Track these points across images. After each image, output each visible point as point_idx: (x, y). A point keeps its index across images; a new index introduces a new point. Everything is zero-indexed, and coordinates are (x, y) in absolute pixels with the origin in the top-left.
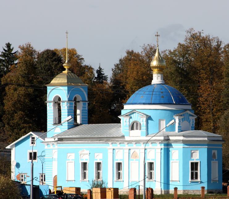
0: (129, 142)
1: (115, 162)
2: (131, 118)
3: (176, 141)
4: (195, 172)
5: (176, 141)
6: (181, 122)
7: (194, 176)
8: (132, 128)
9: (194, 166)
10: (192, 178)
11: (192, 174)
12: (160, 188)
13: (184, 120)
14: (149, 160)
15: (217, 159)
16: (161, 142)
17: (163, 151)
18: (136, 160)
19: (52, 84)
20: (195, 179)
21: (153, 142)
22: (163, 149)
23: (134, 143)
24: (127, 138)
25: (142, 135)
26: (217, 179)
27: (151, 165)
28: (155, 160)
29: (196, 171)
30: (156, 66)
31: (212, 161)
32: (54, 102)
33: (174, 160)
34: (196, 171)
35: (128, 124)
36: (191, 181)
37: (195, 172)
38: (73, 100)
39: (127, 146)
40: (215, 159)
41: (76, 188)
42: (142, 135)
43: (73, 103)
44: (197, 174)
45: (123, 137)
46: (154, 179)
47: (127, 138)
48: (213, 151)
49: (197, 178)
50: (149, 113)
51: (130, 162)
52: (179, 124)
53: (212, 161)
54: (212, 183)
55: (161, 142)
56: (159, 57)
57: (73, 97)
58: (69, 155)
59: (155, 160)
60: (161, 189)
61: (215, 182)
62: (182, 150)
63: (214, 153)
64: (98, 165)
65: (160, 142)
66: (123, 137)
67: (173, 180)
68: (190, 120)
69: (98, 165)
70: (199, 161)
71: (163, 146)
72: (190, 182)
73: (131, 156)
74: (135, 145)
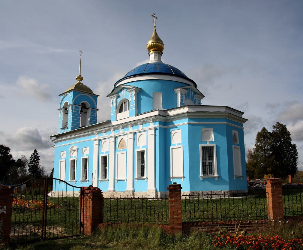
0: (116, 128)
1: (101, 155)
2: (119, 97)
3: (179, 117)
4: (208, 162)
5: (179, 117)
6: (184, 97)
7: (207, 168)
8: (121, 111)
9: (208, 152)
10: (204, 172)
11: (204, 165)
12: (154, 188)
13: (188, 98)
14: (140, 147)
15: (238, 143)
16: (154, 117)
17: (157, 132)
18: (123, 151)
19: (138, 147)
20: (209, 174)
21: (144, 122)
22: (158, 128)
23: (120, 127)
24: (114, 123)
25: (130, 115)
26: (241, 174)
27: (142, 154)
28: (146, 146)
29: (210, 161)
30: (152, 43)
31: (233, 146)
32: (64, 109)
33: (175, 145)
34: (210, 161)
35: (115, 105)
36: (203, 176)
37: (208, 162)
38: (80, 105)
39: (112, 133)
40: (236, 144)
41: (81, 188)
42: (130, 115)
43: (79, 107)
44: (211, 165)
45: (109, 122)
46: (145, 176)
47: (114, 123)
48: (234, 132)
49: (211, 172)
50: (140, 85)
51: (117, 153)
52: (182, 100)
53: (233, 146)
54: (235, 179)
55: (154, 119)
56: (156, 36)
57: (81, 102)
58: (62, 153)
59: (146, 146)
60: (156, 191)
61: (238, 177)
62: (186, 128)
63: (235, 135)
64: (85, 161)
65: (153, 119)
66: (109, 122)
67: (61, 179)
68: (195, 100)
69: (85, 161)
70: (214, 145)
71: (157, 125)
72: (201, 179)
73: (118, 145)
74: (122, 130)
